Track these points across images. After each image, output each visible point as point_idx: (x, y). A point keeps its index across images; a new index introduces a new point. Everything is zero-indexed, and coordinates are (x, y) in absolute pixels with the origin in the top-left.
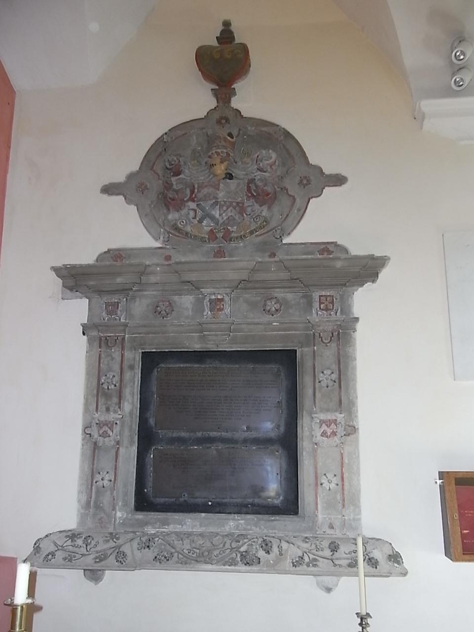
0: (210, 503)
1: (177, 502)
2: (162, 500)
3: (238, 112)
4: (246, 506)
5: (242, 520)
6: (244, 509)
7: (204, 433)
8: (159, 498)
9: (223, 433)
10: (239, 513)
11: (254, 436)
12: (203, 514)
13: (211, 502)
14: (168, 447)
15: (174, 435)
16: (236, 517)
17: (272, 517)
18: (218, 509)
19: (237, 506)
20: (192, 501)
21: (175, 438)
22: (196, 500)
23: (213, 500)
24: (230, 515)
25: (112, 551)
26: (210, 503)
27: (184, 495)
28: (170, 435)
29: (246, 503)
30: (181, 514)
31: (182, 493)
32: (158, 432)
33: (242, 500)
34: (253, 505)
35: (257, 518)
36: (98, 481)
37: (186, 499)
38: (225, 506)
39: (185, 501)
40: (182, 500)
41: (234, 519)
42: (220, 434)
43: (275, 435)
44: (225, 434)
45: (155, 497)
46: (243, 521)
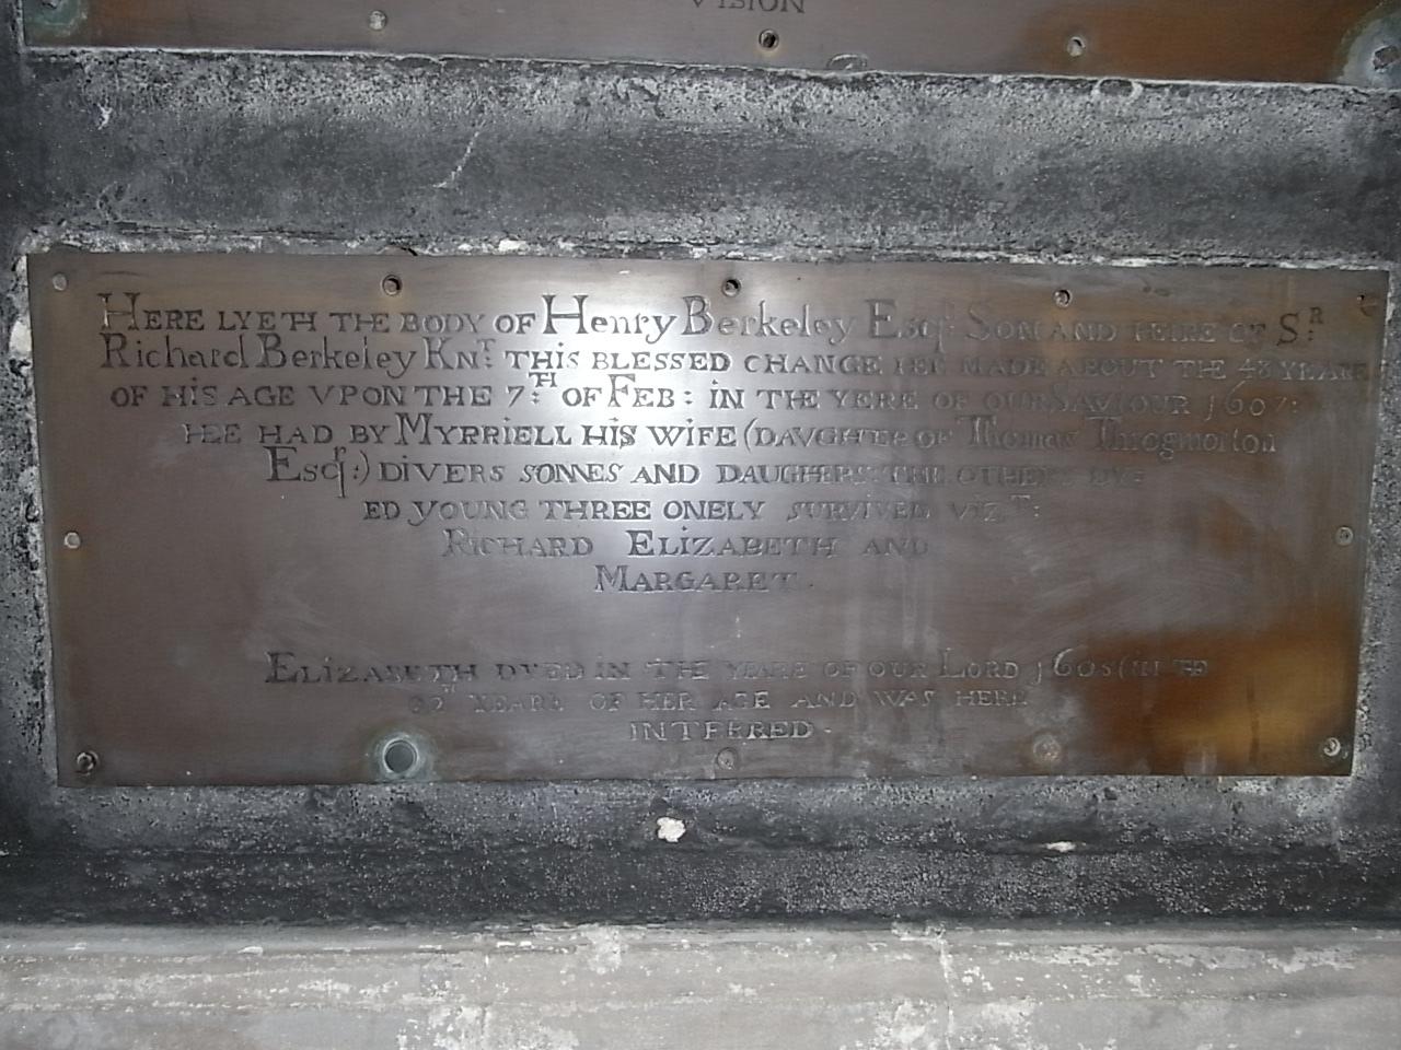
0: (671, 830)
1: (329, 827)
2: (169, 809)
3: (664, 840)
4: (1028, 845)
5: (1005, 992)
6: (1015, 880)
7: (602, 87)
8: (135, 784)
9: (817, 99)
10: (960, 910)
11: (1149, 136)
12: (607, 943)
13: (681, 812)
14: (198, 241)
15: (258, 105)
16: (946, 961)
17: (1286, 952)
18: (752, 883)
19: (945, 844)
20: (478, 809)
21: (272, 132)
22: (525, 801)
23: (704, 799)
24: (873, 940)
25: (582, 469)
26: (671, 830)
27: (399, 759)
28: (213, 98)
29: (1026, 814)
30: (375, 942)
31: (372, 736)
32: (69, 69)
33: (986, 789)
34: (1090, 834)
35: (1151, 966)
36: (388, 427)
37: (423, 792)
38: (825, 844)
39: (412, 808)
40: (377, 796)
41: (928, 992)
42: (779, 100)
43: (1354, 133)
44: (847, 102)
45: (94, 776)
46: (1026, 1007)
